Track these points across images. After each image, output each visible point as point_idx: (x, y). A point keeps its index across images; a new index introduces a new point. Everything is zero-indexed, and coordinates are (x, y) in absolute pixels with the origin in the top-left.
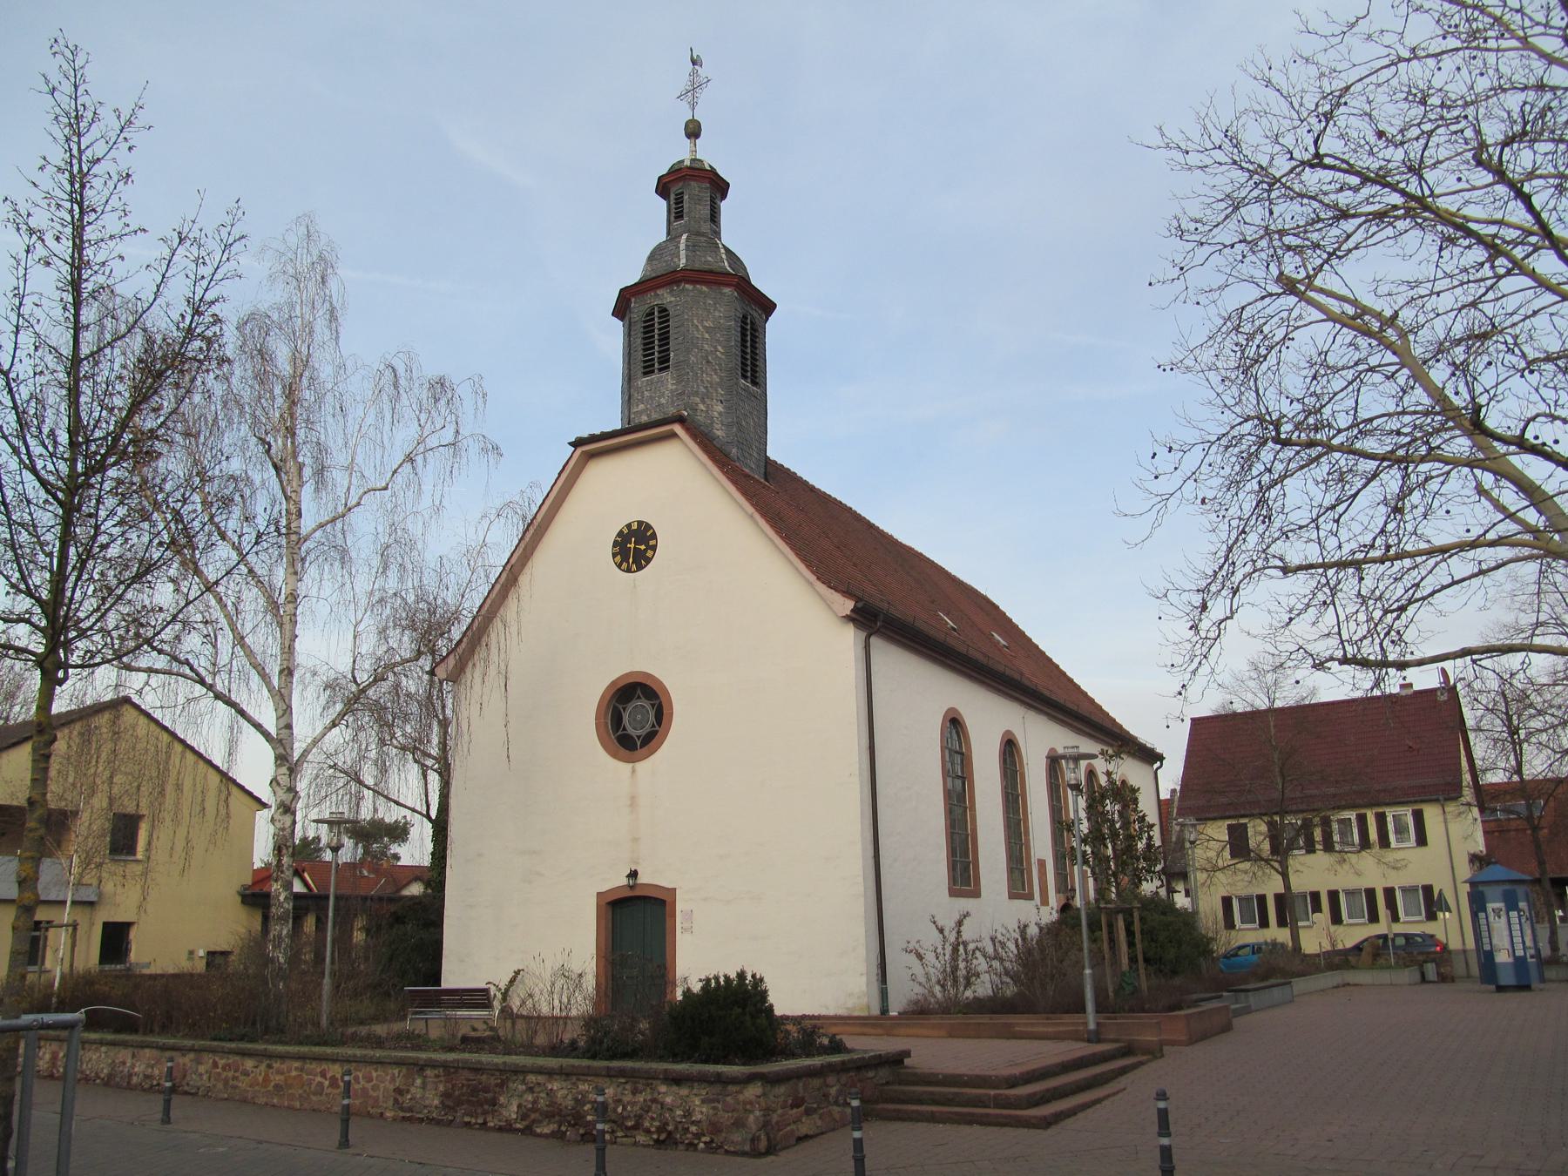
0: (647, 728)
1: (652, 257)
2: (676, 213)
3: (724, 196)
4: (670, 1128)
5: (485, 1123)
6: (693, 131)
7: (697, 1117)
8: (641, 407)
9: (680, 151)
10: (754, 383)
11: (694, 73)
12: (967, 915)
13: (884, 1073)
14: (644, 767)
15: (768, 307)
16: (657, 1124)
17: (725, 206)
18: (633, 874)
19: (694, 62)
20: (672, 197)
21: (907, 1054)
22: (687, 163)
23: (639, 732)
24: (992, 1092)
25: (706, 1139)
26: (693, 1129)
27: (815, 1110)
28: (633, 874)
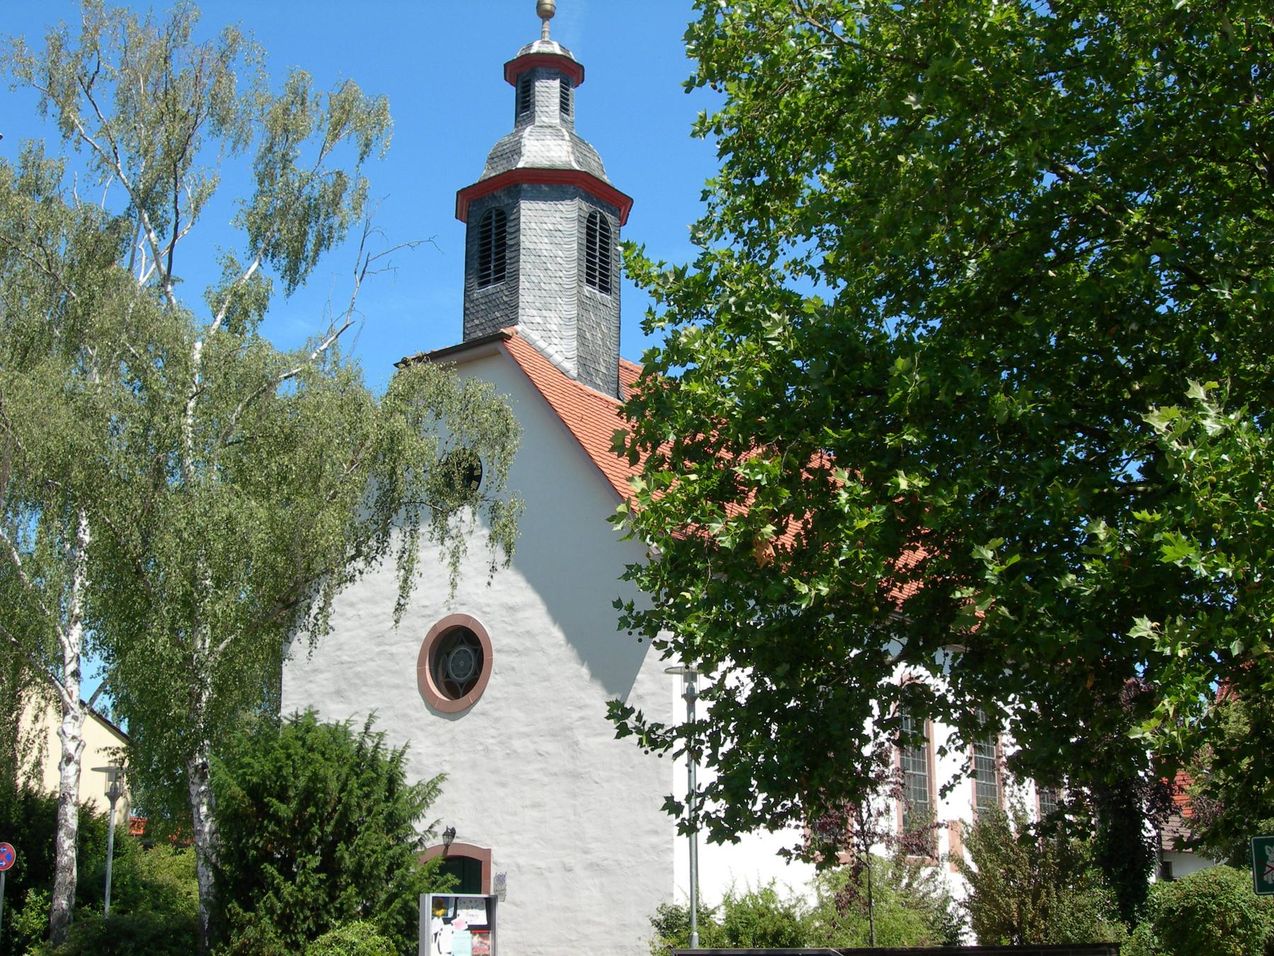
8: (477, 322)
10: (605, 288)
23: (462, 679)
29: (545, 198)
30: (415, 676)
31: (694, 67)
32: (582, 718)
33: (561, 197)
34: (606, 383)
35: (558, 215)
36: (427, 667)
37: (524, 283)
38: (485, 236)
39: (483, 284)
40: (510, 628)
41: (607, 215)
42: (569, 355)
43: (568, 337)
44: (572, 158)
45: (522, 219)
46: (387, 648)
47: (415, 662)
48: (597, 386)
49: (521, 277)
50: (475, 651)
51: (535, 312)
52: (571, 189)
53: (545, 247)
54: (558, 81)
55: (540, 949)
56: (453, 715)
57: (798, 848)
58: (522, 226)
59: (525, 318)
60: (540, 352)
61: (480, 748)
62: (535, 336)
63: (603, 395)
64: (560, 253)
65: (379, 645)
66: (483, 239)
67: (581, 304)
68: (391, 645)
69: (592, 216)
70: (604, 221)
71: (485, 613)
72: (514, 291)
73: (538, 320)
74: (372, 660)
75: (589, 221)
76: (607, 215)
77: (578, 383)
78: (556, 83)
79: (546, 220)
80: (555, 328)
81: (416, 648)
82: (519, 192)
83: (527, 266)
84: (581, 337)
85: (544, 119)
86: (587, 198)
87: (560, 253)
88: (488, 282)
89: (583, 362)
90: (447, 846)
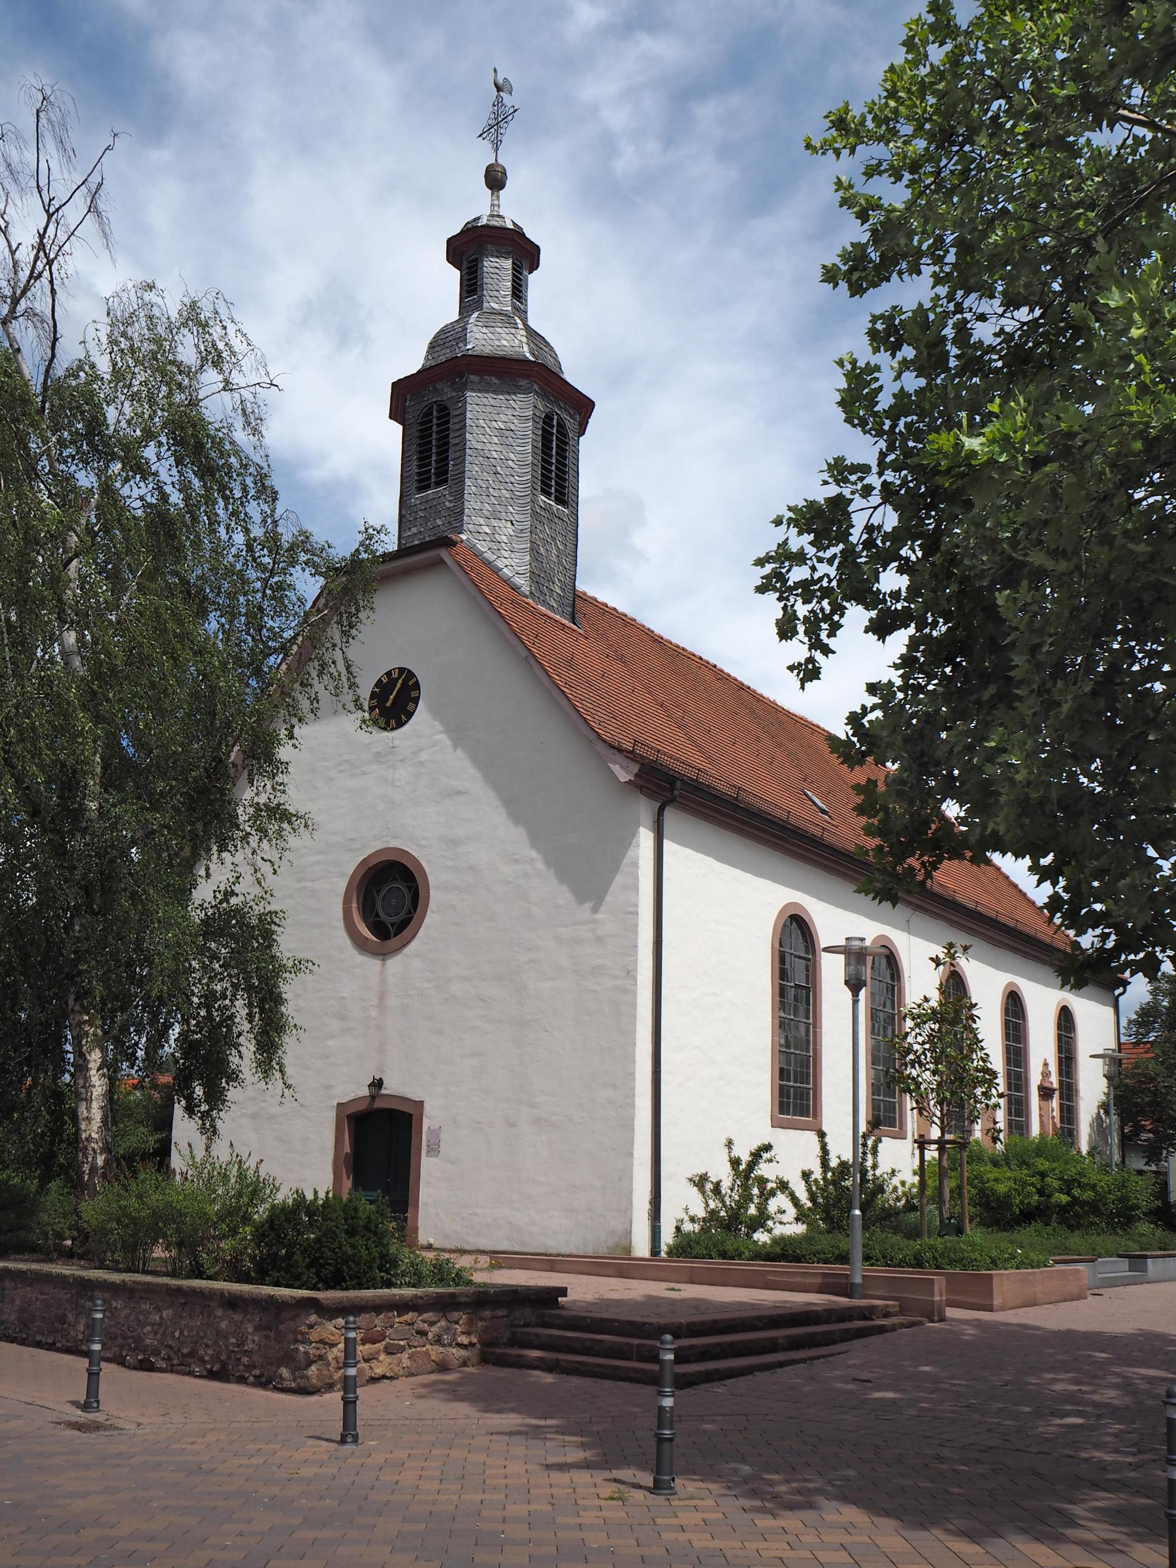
0: (403, 914)
1: (433, 346)
2: (471, 288)
3: (534, 265)
4: (224, 1357)
5: (54, 1343)
6: (495, 180)
7: (250, 1346)
8: (414, 530)
9: (476, 205)
10: (560, 500)
11: (499, 102)
12: (767, 1148)
13: (527, 1313)
14: (395, 963)
15: (583, 407)
16: (210, 1352)
17: (534, 280)
18: (377, 1084)
19: (499, 89)
20: (464, 267)
21: (563, 1292)
22: (483, 221)
23: (393, 919)
24: (636, 1342)
25: (257, 1372)
26: (245, 1360)
27: (402, 1349)
28: (377, 1084)
29: (497, 391)
30: (340, 914)
31: (860, 221)
32: (532, 961)
33: (513, 390)
34: (561, 605)
35: (509, 412)
36: (354, 905)
37: (470, 487)
38: (425, 434)
39: (421, 489)
40: (450, 864)
41: (564, 416)
42: (521, 569)
43: (521, 550)
44: (526, 348)
45: (469, 415)
46: (308, 884)
47: (340, 900)
48: (551, 608)
49: (468, 482)
50: (409, 888)
51: (482, 521)
52: (523, 382)
53: (494, 448)
54: (510, 262)
55: (477, 1210)
56: (383, 955)
57: (780, 599)
58: (468, 422)
59: (471, 526)
60: (488, 564)
61: (413, 992)
62: (482, 547)
63: (558, 617)
64: (512, 456)
65: (299, 881)
66: (421, 438)
67: (534, 514)
68: (313, 881)
69: (548, 420)
70: (561, 425)
71: (420, 846)
72: (459, 496)
73: (487, 530)
74: (291, 897)
75: (544, 422)
76: (564, 416)
77: (530, 601)
78: (508, 264)
79: (496, 417)
80: (504, 539)
81: (342, 885)
82: (465, 384)
83: (473, 468)
84: (534, 550)
85: (493, 305)
86: (544, 395)
87: (512, 456)
88: (428, 487)
89: (534, 577)
90: (373, 1097)
